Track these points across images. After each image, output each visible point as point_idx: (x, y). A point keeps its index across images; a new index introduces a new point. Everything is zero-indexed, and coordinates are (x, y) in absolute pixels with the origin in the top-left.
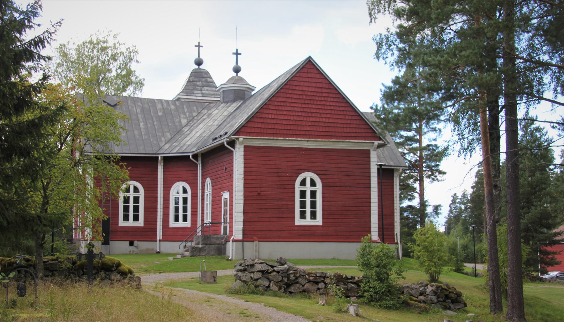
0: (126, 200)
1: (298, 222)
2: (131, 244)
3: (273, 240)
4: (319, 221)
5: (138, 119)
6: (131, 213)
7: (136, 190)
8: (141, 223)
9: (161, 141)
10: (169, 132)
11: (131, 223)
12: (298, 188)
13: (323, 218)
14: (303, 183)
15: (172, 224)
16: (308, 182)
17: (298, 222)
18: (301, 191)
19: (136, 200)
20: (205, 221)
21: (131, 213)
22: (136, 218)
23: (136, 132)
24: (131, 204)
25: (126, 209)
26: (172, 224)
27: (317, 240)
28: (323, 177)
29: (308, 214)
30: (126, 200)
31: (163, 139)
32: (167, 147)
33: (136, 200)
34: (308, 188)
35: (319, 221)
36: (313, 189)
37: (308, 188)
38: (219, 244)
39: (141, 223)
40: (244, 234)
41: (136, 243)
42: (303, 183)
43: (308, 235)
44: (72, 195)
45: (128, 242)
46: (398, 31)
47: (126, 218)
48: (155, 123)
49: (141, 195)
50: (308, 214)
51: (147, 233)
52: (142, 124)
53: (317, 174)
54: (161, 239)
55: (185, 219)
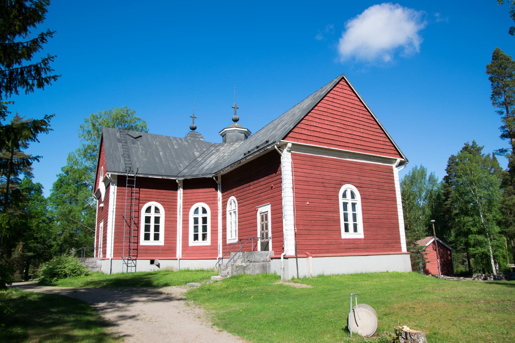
0: (148, 219)
1: (344, 235)
2: (152, 262)
3: (196, 258)
4: (360, 234)
5: (158, 150)
6: (152, 232)
7: (157, 210)
8: (161, 243)
9: (180, 167)
10: (186, 160)
11: (152, 242)
12: (143, 215)
13: (365, 230)
14: (148, 210)
15: (192, 243)
16: (153, 210)
17: (344, 235)
18: (146, 217)
19: (157, 220)
20: (228, 237)
21: (152, 232)
22: (157, 237)
23: (157, 159)
24: (152, 224)
25: (147, 228)
26: (192, 243)
27: (366, 254)
28: (361, 189)
29: (152, 236)
30: (148, 219)
31: (181, 165)
32: (186, 171)
33: (205, 220)
34: (153, 215)
35: (360, 234)
36: (157, 215)
37: (200, 215)
38: (264, 261)
39: (161, 243)
40: (296, 250)
41: (157, 261)
42: (148, 210)
43: (353, 248)
44: (457, 195)
45: (149, 261)
46: (39, 132)
47: (147, 237)
48: (173, 153)
49: (208, 215)
50: (152, 236)
51: (168, 251)
52: (161, 153)
53: (357, 187)
54: (181, 257)
55: (157, 237)
